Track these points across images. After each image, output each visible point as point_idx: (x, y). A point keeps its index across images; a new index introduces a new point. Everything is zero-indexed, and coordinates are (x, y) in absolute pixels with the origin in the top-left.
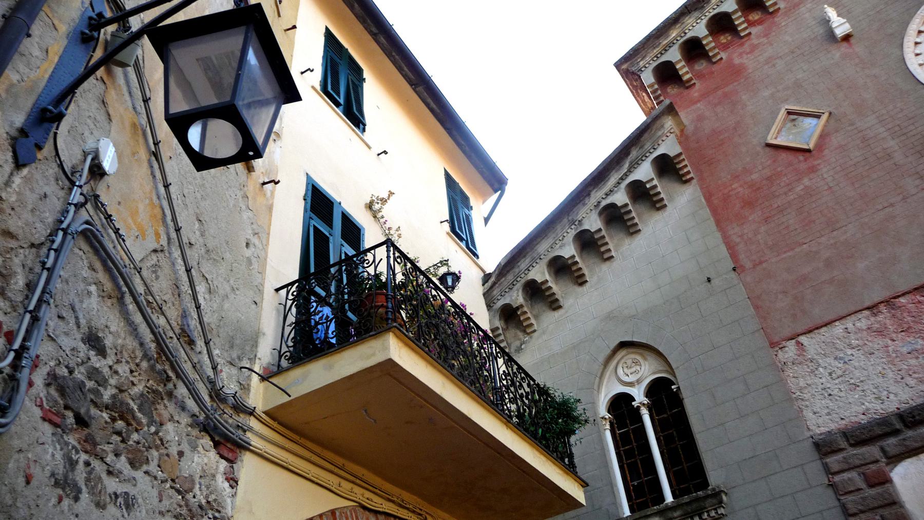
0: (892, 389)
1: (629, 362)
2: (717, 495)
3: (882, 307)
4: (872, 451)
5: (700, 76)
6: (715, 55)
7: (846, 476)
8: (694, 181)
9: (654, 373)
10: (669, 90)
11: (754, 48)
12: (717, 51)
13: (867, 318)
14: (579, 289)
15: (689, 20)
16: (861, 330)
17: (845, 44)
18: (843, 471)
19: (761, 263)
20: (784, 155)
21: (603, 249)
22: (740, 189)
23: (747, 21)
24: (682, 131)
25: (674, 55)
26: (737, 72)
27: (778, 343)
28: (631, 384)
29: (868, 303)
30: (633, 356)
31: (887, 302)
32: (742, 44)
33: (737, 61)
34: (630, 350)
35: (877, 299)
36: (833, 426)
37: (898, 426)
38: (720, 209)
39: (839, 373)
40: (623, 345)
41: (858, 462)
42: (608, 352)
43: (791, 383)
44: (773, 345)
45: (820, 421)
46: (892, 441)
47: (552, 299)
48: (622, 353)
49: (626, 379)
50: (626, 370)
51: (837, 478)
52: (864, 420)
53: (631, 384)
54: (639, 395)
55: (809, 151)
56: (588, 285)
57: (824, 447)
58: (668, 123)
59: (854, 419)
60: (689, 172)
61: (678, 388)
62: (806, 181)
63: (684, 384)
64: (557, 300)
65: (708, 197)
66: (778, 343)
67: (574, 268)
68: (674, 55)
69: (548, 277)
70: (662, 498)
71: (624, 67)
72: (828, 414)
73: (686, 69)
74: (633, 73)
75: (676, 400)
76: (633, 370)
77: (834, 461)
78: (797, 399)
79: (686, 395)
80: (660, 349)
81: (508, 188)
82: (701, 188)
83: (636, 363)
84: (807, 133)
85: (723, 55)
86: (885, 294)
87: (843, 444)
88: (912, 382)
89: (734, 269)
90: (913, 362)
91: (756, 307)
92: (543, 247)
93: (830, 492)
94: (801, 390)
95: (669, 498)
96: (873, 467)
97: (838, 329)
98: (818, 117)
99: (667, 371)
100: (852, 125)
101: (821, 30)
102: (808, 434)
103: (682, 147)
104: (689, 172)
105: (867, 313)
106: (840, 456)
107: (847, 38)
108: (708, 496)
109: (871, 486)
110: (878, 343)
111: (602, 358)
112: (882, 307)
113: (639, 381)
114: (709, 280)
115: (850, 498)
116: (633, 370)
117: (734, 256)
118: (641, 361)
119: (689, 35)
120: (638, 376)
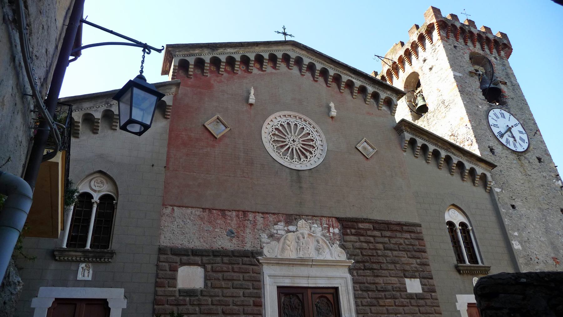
0: (195, 240)
1: (99, 181)
2: (112, 253)
3: (207, 210)
4: (177, 259)
5: (195, 75)
6: (206, 73)
7: (164, 264)
8: (169, 120)
9: (108, 191)
10: (180, 72)
11: (221, 82)
12: (208, 72)
13: (201, 212)
14: (92, 135)
15: (206, 51)
16: (196, 215)
17: (249, 106)
18: (164, 262)
19: (176, 170)
20: (207, 134)
21: (114, 124)
22: (184, 136)
23: (225, 69)
24: (176, 94)
25: (191, 60)
26: (209, 86)
27: (166, 205)
28: (95, 191)
29: (203, 207)
30: (102, 179)
31: (210, 210)
32: (218, 76)
33: (212, 82)
34: (102, 176)
35: (207, 207)
36: (169, 245)
37: (190, 253)
38: (173, 139)
39: (181, 226)
40: (100, 172)
41: (170, 261)
42: (92, 172)
43: (163, 222)
44: (164, 205)
45: (165, 241)
46: (185, 258)
47: (77, 132)
48: (98, 175)
49: (94, 188)
50: (95, 183)
51: (161, 264)
52: (180, 246)
53: (95, 191)
54: (96, 198)
55: (216, 138)
56: (97, 135)
57: (162, 251)
58: (174, 89)
59: (177, 245)
60: (169, 115)
61: (117, 203)
62: (209, 149)
63: (121, 202)
64: (79, 134)
65: (171, 130)
66: (166, 205)
67: (96, 124)
68: (191, 60)
69: (80, 121)
70: (85, 245)
71: (170, 49)
72: (169, 240)
73: (192, 70)
74: (171, 54)
75: (113, 208)
76: (99, 185)
77: (163, 257)
78: (161, 229)
79: (119, 207)
80: (117, 183)
81: (79, 58)
82: (170, 125)
83: (102, 182)
84: (219, 130)
85: (209, 75)
86: (211, 207)
87: (169, 252)
88: (202, 240)
89: (165, 167)
90: (206, 234)
91: (165, 187)
92: (86, 105)
93: (155, 268)
94: (164, 227)
95: (88, 247)
96: (175, 264)
97: (189, 211)
98: (226, 128)
99: (114, 193)
100: (235, 138)
101: (245, 94)
102: (158, 244)
103: (173, 104)
104: (169, 115)
105: (201, 210)
106: (165, 256)
107: (251, 105)
108: (108, 253)
109: (170, 270)
110: (200, 222)
111: (87, 173)
112: (207, 210)
113: (99, 191)
114: (153, 166)
115: (162, 272)
116: (99, 185)
117: (168, 161)
118: (105, 183)
119: (202, 57)
120: (100, 189)
